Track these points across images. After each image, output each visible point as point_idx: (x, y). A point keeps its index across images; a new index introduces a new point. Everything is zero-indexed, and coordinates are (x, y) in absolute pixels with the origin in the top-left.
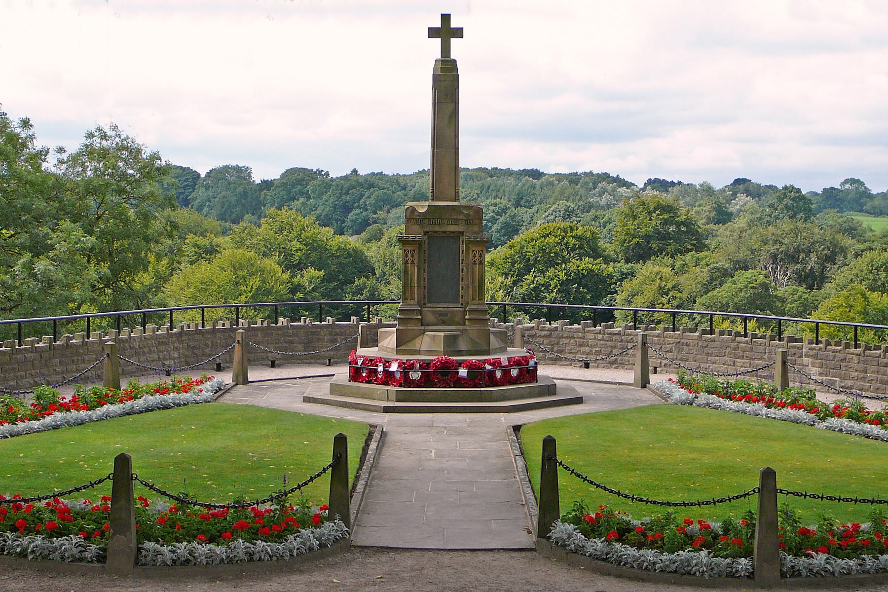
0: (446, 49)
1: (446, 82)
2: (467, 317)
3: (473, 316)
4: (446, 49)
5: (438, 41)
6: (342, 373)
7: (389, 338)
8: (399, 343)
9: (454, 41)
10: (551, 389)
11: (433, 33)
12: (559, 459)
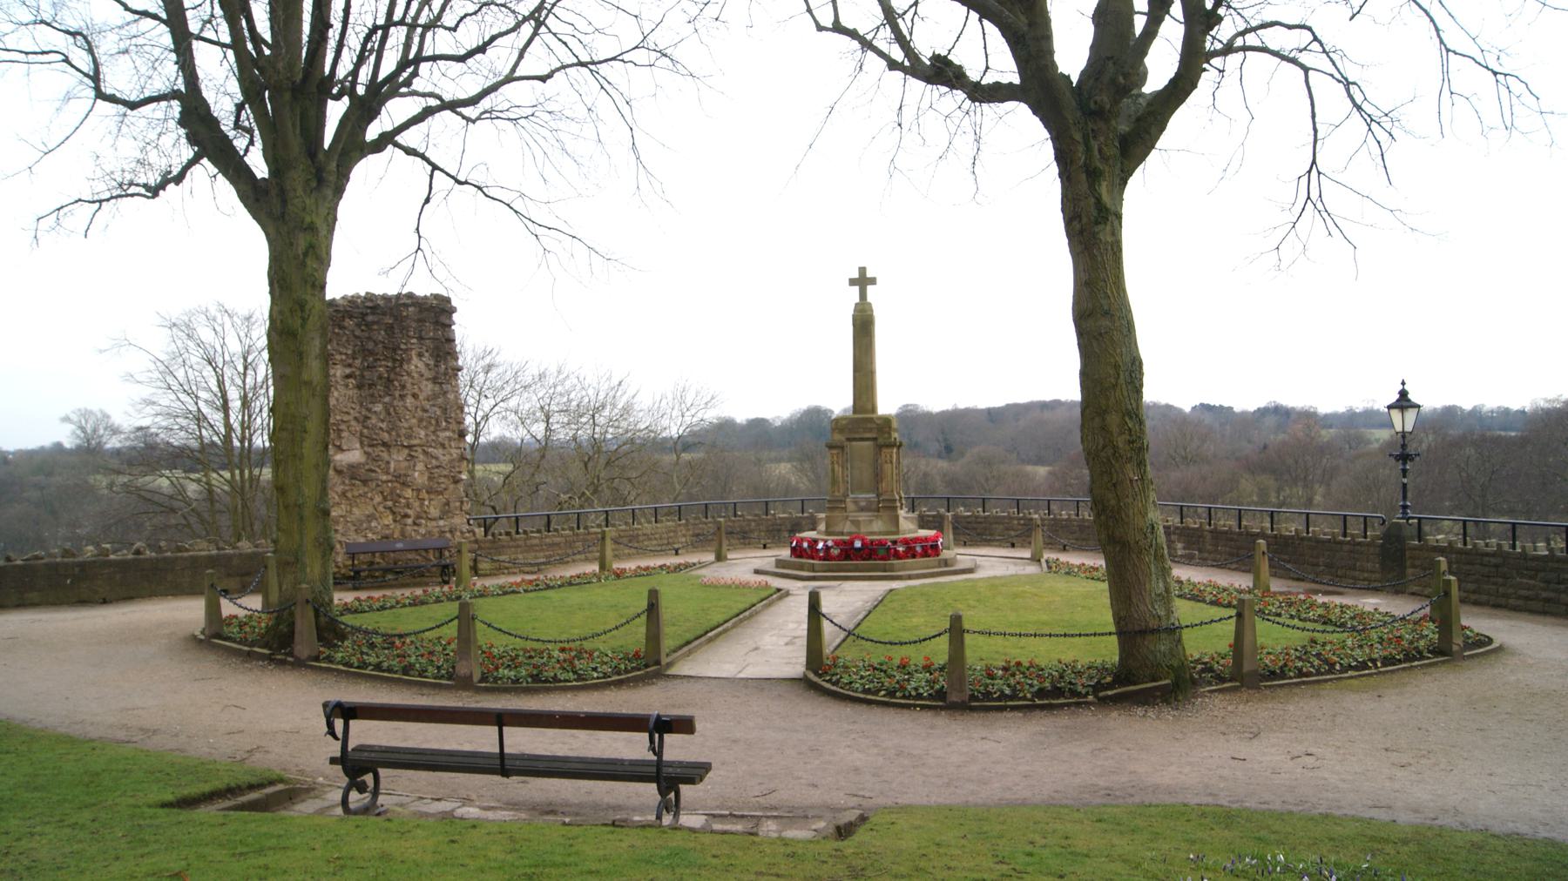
0: (863, 295)
1: (863, 326)
4: (863, 295)
5: (856, 289)
6: (785, 553)
9: (869, 288)
11: (852, 282)
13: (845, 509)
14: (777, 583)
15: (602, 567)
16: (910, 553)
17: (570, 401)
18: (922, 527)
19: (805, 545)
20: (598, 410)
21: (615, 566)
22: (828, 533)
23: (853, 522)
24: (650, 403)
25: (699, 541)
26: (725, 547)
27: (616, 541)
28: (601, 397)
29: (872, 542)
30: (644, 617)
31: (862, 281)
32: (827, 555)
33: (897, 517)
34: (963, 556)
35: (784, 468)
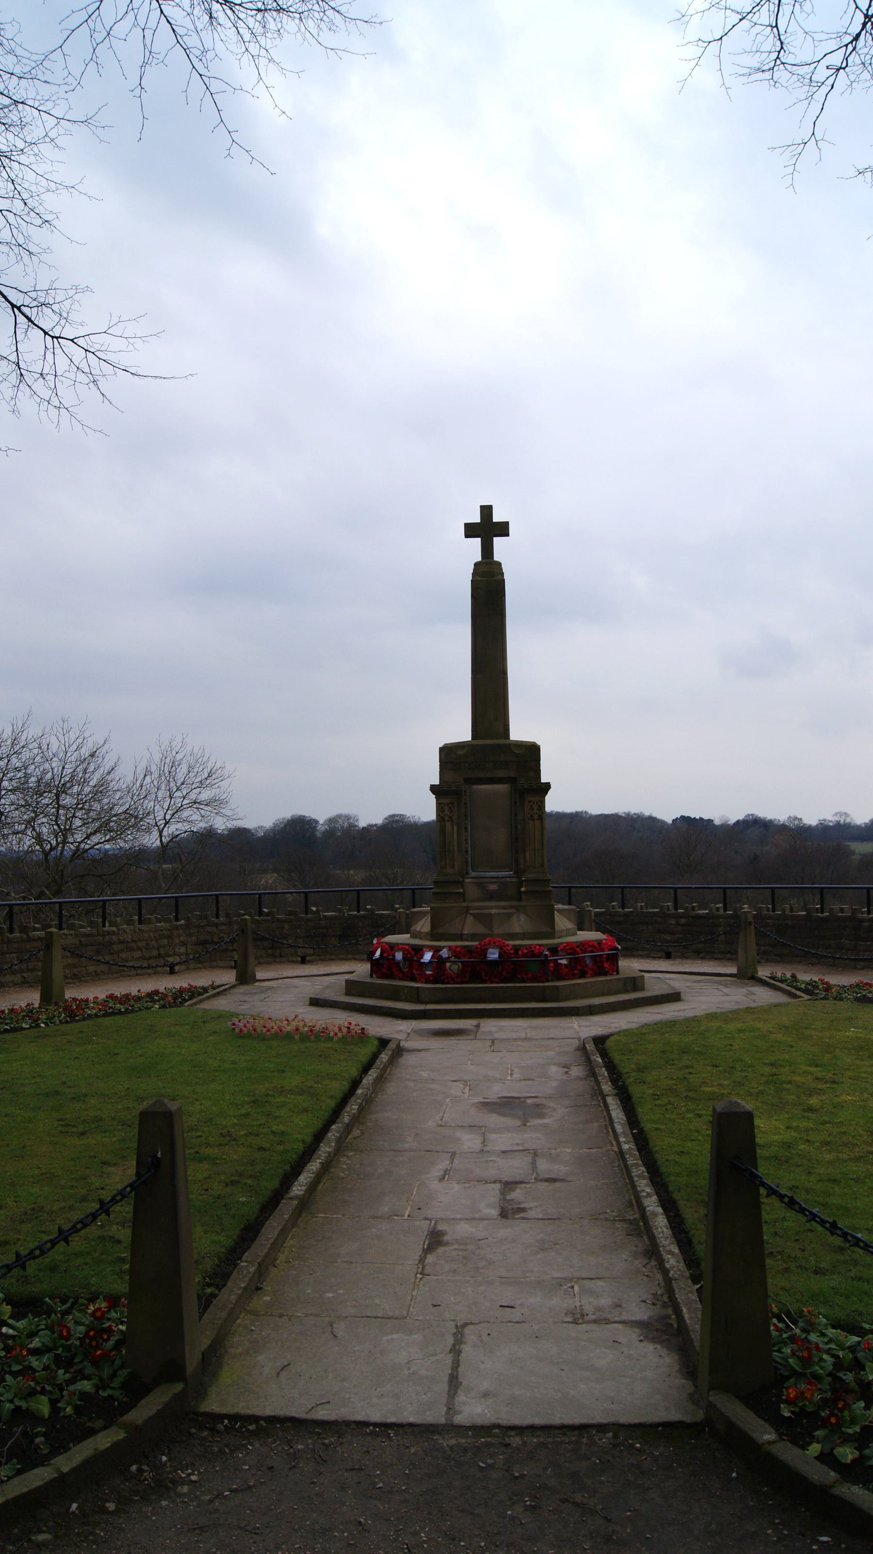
0: (487, 550)
1: (488, 593)
2: (523, 889)
4: (487, 550)
6: (361, 969)
7: (423, 920)
8: (433, 925)
9: (497, 541)
11: (471, 530)
12: (764, 1170)
13: (462, 896)
14: (378, 1027)
15: (46, 998)
16: (577, 969)
17: (27, 776)
19: (399, 956)
20: (62, 790)
21: (69, 994)
23: (479, 917)
24: (130, 778)
25: (206, 955)
26: (251, 959)
27: (73, 952)
28: (68, 770)
29: (516, 949)
30: (125, 1210)
31: (487, 529)
34: (656, 972)
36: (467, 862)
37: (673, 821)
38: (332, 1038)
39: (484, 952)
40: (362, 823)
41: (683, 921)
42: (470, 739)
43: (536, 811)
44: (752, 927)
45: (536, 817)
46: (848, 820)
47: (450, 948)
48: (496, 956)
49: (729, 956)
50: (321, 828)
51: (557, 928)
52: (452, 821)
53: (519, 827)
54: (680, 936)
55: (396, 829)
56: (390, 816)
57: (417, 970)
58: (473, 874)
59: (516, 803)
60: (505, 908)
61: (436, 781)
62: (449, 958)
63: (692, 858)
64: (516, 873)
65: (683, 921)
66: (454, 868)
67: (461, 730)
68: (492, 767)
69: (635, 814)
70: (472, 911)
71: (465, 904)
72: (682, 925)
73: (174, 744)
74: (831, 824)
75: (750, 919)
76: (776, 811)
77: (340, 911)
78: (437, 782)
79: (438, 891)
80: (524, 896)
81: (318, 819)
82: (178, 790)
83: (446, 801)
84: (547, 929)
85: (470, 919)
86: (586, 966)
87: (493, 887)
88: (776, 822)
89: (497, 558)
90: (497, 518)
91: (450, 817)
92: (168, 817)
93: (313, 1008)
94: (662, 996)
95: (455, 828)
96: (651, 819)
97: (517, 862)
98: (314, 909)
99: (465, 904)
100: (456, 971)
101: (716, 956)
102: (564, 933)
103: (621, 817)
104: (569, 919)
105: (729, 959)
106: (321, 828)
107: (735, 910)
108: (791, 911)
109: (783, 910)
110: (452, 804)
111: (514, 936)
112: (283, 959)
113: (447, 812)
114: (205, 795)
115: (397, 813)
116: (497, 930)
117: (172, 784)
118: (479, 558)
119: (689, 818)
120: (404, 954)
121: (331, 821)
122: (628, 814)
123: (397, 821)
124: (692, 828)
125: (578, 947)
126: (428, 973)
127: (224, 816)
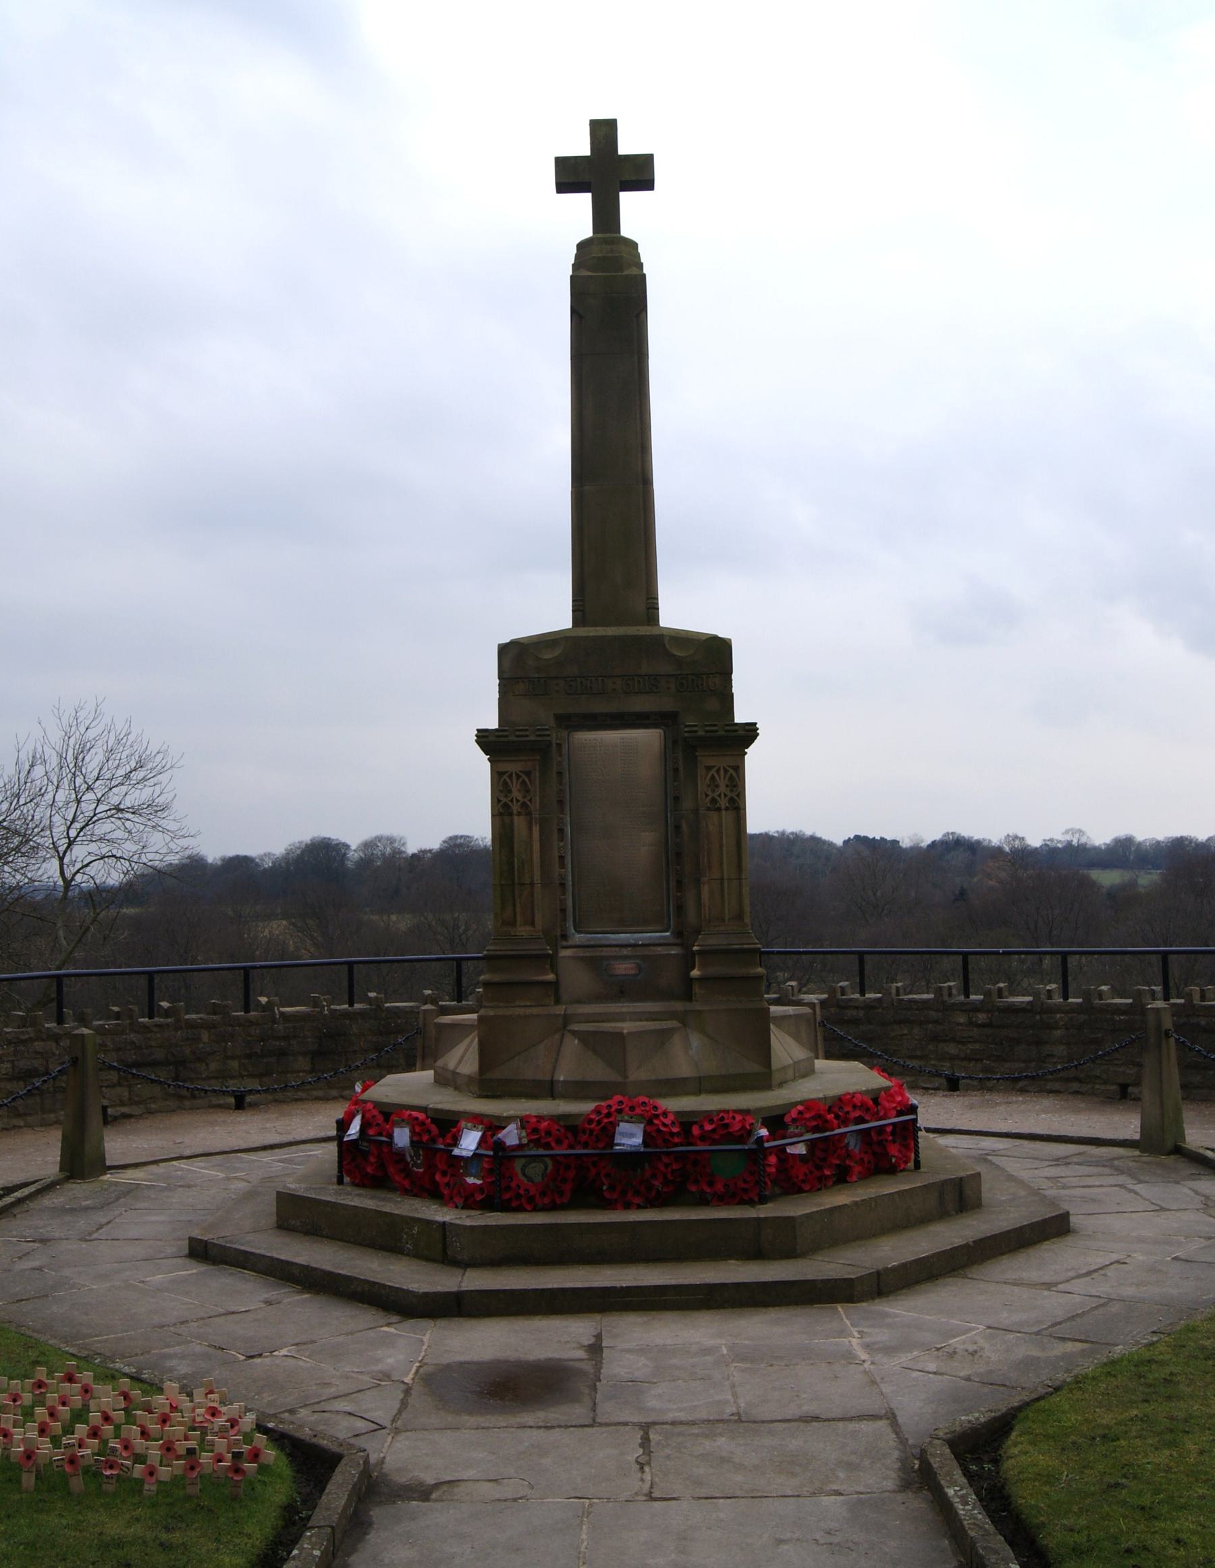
0: (606, 216)
1: (609, 305)
2: (695, 973)
3: (713, 970)
4: (606, 216)
5: (582, 203)
8: (487, 1058)
9: (627, 199)
10: (960, 1196)
11: (570, 175)
16: (828, 1166)
18: (837, 1050)
19: (402, 1137)
22: (487, 1086)
23: (592, 1041)
26: (95, 1118)
29: (686, 1122)
31: (605, 171)
32: (499, 1179)
33: (764, 1019)
35: (276, 928)
36: (563, 911)
37: (846, 842)
38: (140, 1482)
39: (608, 1134)
40: (411, 849)
41: (982, 1017)
42: (568, 624)
43: (722, 789)
44: (1172, 1040)
45: (723, 803)
46: (1083, 840)
47: (524, 1122)
48: (638, 1140)
49: (1075, 1086)
50: (354, 855)
51: (775, 1064)
52: (529, 814)
53: (685, 827)
54: (977, 1046)
55: (456, 854)
56: (451, 838)
57: (444, 1174)
58: (579, 938)
59: (676, 770)
60: (652, 1017)
61: (492, 722)
62: (520, 1147)
63: (879, 894)
64: (679, 934)
65: (982, 1017)
66: (533, 924)
67: (549, 608)
68: (616, 696)
69: (792, 833)
70: (575, 1027)
71: (560, 1010)
72: (979, 1026)
73: (82, 714)
74: (1060, 846)
75: (1168, 1023)
76: (990, 827)
77: (316, 1003)
78: (492, 723)
79: (496, 978)
80: (697, 989)
81: (348, 843)
82: (89, 788)
83: (513, 767)
84: (753, 1067)
85: (572, 1045)
86: (849, 1155)
87: (624, 968)
88: (985, 844)
89: (626, 231)
90: (627, 146)
91: (524, 805)
92: (73, 833)
93: (195, 1269)
94: (1032, 1226)
95: (536, 830)
96: (814, 839)
97: (680, 909)
98: (264, 1000)
99: (560, 1010)
100: (538, 1179)
101: (1049, 1086)
102: (790, 1073)
103: (773, 837)
104: (796, 1037)
105: (1076, 1093)
106: (354, 855)
107: (1087, 995)
108: (1203, 998)
109: (1189, 996)
110: (528, 774)
111: (676, 1087)
112: (198, 1102)
113: (516, 794)
114: (135, 797)
115: (460, 833)
116: (638, 1074)
117: (79, 781)
118: (587, 232)
119: (866, 838)
120: (413, 1132)
121: (368, 845)
122: (783, 833)
123: (461, 845)
124: (872, 855)
125: (830, 1110)
126: (470, 1180)
127: (164, 831)
